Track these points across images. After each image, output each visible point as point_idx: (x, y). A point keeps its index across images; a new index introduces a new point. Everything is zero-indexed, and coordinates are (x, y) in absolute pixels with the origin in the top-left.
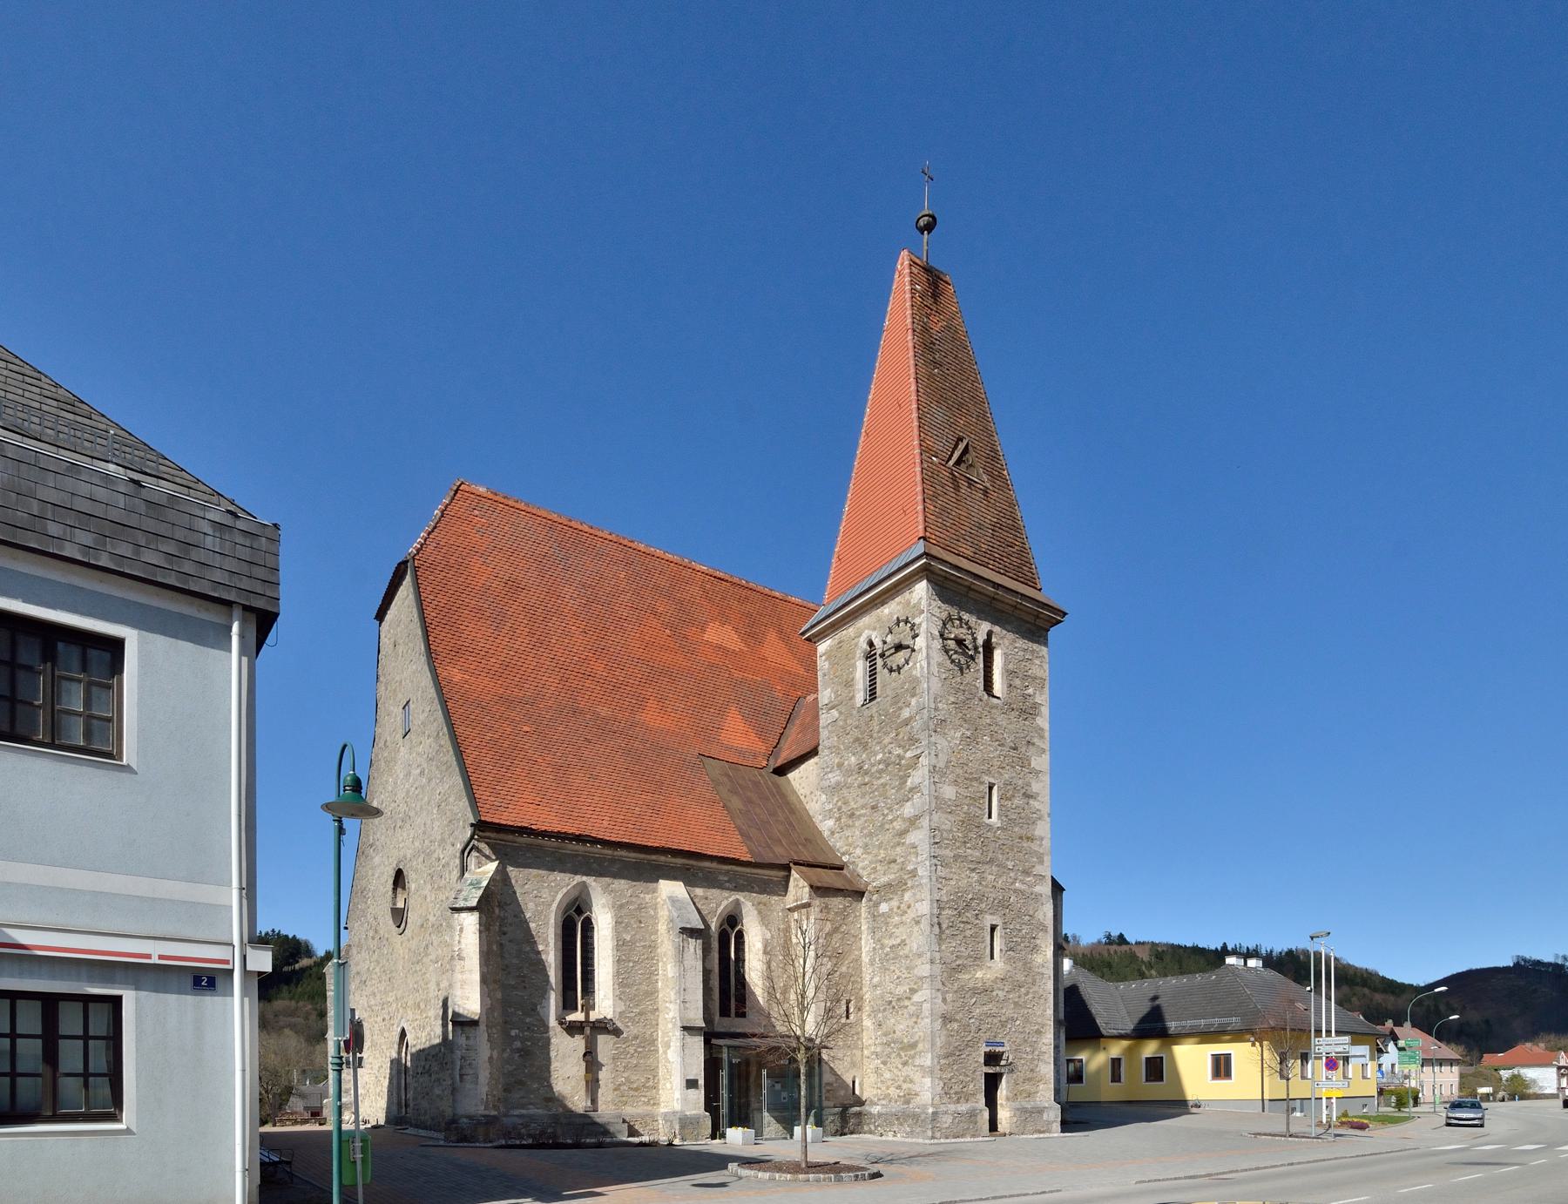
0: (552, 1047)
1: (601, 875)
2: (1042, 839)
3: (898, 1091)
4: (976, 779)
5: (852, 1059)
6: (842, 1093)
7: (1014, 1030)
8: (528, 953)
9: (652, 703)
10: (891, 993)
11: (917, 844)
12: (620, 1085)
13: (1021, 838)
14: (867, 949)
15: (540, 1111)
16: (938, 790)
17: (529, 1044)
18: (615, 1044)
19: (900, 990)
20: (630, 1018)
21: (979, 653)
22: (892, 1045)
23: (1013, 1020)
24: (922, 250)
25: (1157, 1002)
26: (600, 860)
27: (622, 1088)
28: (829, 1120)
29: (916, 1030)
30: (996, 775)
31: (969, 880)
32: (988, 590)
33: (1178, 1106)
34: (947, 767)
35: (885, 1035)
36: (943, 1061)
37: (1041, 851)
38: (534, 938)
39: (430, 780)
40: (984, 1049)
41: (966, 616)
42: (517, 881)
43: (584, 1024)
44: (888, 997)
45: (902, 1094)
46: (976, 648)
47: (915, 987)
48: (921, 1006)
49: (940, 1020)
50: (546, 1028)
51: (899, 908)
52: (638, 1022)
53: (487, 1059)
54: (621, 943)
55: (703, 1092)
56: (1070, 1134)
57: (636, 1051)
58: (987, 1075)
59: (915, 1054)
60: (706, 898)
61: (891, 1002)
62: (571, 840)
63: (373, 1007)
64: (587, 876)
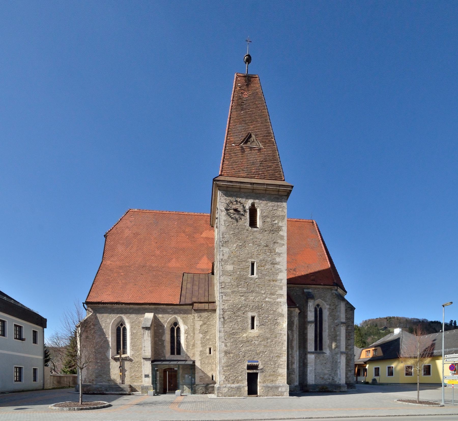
0: (111, 365)
1: (126, 313)
2: (281, 280)
4: (244, 261)
5: (211, 368)
6: (207, 379)
7: (264, 356)
9: (174, 260)
12: (132, 376)
13: (269, 281)
15: (107, 384)
16: (224, 267)
20: (136, 356)
21: (247, 212)
23: (263, 352)
24: (246, 69)
25: (435, 342)
26: (126, 309)
27: (133, 377)
30: (255, 258)
31: (240, 300)
33: (438, 385)
34: (228, 258)
36: (225, 368)
37: (281, 285)
38: (105, 333)
40: (247, 363)
41: (239, 200)
42: (99, 318)
46: (245, 211)
49: (224, 353)
50: (109, 360)
52: (138, 357)
56: (292, 397)
57: (138, 366)
58: (248, 374)
60: (163, 317)
62: (114, 304)
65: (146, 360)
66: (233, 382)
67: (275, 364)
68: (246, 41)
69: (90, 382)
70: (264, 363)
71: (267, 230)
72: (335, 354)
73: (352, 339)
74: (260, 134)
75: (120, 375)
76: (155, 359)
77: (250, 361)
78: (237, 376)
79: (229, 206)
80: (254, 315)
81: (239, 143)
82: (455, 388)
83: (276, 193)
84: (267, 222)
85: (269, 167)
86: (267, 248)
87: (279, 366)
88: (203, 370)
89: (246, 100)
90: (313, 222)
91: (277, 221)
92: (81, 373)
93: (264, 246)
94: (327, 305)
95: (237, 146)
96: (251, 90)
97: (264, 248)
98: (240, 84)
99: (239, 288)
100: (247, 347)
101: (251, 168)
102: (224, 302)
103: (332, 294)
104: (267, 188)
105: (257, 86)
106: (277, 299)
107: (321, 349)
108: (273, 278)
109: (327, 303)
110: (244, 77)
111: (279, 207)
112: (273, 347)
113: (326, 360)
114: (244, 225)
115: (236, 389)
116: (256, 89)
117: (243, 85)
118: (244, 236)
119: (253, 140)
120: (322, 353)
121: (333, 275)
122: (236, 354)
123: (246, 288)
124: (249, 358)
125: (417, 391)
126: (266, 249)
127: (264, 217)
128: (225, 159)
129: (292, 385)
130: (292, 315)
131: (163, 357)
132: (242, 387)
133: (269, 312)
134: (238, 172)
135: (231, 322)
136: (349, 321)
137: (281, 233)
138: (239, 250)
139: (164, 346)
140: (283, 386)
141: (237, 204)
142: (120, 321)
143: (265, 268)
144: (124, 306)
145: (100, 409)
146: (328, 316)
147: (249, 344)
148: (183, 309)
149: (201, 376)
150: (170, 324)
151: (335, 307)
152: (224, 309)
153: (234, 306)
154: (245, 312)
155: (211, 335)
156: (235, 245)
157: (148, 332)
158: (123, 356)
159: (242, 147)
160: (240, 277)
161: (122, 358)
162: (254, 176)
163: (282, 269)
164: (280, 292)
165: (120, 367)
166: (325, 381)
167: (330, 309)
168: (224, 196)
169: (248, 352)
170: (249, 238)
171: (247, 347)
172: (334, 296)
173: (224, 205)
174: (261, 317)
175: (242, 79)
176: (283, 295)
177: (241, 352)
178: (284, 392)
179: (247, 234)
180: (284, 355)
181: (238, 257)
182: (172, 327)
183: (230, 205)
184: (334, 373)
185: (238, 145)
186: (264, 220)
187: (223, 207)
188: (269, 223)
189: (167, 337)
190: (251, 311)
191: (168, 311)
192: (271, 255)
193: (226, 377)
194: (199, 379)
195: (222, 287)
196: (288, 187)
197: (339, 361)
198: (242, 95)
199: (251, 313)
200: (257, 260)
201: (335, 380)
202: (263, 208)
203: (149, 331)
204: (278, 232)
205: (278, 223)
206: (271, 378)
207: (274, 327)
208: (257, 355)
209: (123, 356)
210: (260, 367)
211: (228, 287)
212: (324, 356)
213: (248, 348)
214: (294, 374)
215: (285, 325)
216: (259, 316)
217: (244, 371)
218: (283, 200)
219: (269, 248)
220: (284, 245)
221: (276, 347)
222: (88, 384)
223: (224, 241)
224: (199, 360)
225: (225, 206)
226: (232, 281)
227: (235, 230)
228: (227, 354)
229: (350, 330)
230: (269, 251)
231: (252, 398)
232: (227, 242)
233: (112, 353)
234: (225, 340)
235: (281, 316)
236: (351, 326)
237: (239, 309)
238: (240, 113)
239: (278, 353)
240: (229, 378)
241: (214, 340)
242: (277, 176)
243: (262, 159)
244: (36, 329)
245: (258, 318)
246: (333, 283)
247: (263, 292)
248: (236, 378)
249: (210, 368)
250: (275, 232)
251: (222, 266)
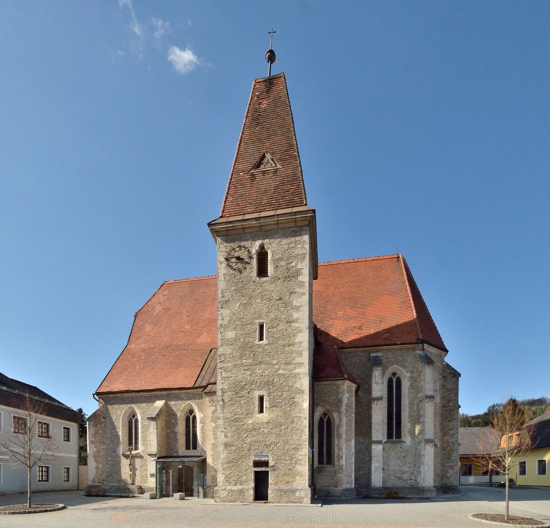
0: (121, 463)
1: (137, 403)
2: (301, 343)
4: (250, 324)
7: (276, 448)
8: (114, 432)
12: (143, 476)
13: (283, 346)
16: (223, 335)
17: (114, 462)
18: (141, 461)
21: (253, 258)
26: (136, 398)
27: (143, 477)
28: (211, 491)
30: (265, 317)
31: (244, 375)
32: (252, 224)
34: (229, 323)
36: (225, 466)
37: (300, 349)
38: (116, 427)
40: (253, 458)
41: (242, 244)
46: (251, 257)
49: (223, 446)
54: (143, 426)
58: (256, 473)
60: (176, 405)
62: (124, 393)
64: (132, 404)
65: (152, 456)
66: (236, 483)
67: (292, 459)
68: (269, 33)
69: (99, 482)
70: (276, 458)
71: (280, 277)
72: (419, 443)
73: (454, 419)
74: (278, 150)
75: (130, 474)
76: (167, 455)
77: (257, 456)
78: (241, 476)
79: (231, 255)
80: (263, 393)
81: (249, 170)
83: (293, 225)
84: (281, 266)
85: (286, 192)
86: (281, 302)
87: (298, 462)
88: (215, 468)
89: (264, 110)
90: (398, 257)
91: (294, 263)
92: (30, 472)
93: (276, 300)
94: (407, 372)
95: (246, 174)
96: (272, 95)
97: (277, 303)
98: (258, 92)
99: (243, 360)
100: (253, 436)
101: (261, 199)
102: (224, 380)
103: (415, 355)
104: (278, 220)
105: (281, 88)
106: (295, 370)
107: (399, 436)
108: (290, 342)
109: (407, 369)
110: (264, 82)
111: (298, 243)
112: (288, 435)
113: (405, 452)
114: (249, 276)
115: (238, 493)
116: (279, 92)
117: (263, 92)
118: (250, 291)
119: (268, 161)
120: (399, 442)
121: (418, 327)
122: (239, 447)
123: (253, 359)
124: (256, 451)
125: (505, 502)
126: (279, 303)
127: (276, 261)
128: (228, 195)
129: (340, 488)
130: (340, 390)
131: (176, 452)
132: (245, 490)
133: (283, 388)
134: (243, 208)
135: (232, 406)
136: (450, 393)
137: (300, 278)
138: (243, 310)
139: (177, 439)
140: (302, 490)
141: (240, 250)
142: (132, 412)
143: (278, 329)
144: (135, 394)
145: (39, 513)
146: (409, 389)
147: (255, 433)
148: (198, 392)
149: (213, 476)
150: (185, 413)
151: (418, 374)
152: (223, 390)
153: (236, 384)
154: (250, 391)
156: (238, 305)
157: (154, 424)
158: (134, 452)
159: (252, 174)
160: (244, 345)
161: (132, 454)
162: (264, 208)
163: (301, 328)
164: (298, 360)
165: (130, 465)
166: (403, 483)
167: (411, 377)
168: (224, 243)
169: (254, 444)
170: (256, 292)
171: (253, 436)
172: (417, 358)
173: (224, 254)
174: (272, 397)
175: (262, 84)
176: (303, 363)
177: (245, 443)
178: (304, 498)
179: (253, 287)
180: (304, 446)
181: (242, 320)
182: (188, 416)
183: (232, 254)
184: (417, 471)
185: (247, 172)
186: (277, 265)
187: (222, 258)
188: (284, 267)
189: (181, 428)
190: (259, 389)
191: (181, 397)
192: (286, 311)
193: (226, 477)
194: (211, 479)
195: (221, 360)
196: (309, 213)
197: (422, 453)
198: (260, 106)
199: (258, 392)
200: (267, 320)
201: (419, 481)
202: (275, 249)
203: (155, 422)
204: (297, 277)
205: (296, 265)
206: (286, 478)
207: (289, 408)
208: (267, 447)
209: (134, 452)
210: (271, 463)
211: (229, 359)
212: (403, 447)
213: (254, 439)
214: (342, 472)
215: (306, 405)
216: (269, 395)
217: (250, 469)
218: (303, 232)
219: (284, 302)
220: (304, 294)
221: (293, 436)
222: (98, 484)
223: (224, 300)
224: (211, 455)
225: (225, 255)
226: (234, 352)
227: (238, 284)
228: (228, 446)
229: (451, 406)
230: (284, 306)
231: (260, 505)
232: (228, 302)
233: (122, 450)
234: (225, 428)
235: (299, 393)
236: (454, 400)
237: (243, 388)
238: (255, 130)
239: (296, 444)
240: (231, 478)
242: (296, 202)
243: (277, 183)
244: (68, 426)
245: (268, 398)
246: (416, 340)
247: (275, 362)
248: (240, 478)
250: (292, 278)
251: (221, 333)
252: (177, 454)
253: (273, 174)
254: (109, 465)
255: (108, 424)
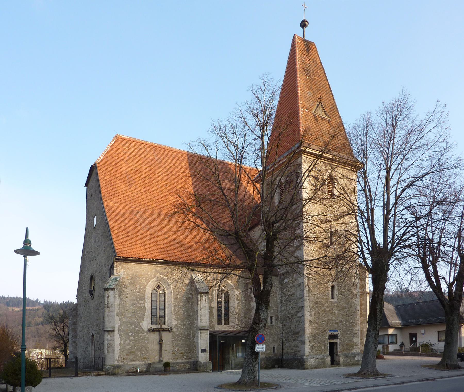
3: (292, 350)
8: (137, 304)
10: (289, 313)
11: (299, 256)
14: (279, 297)
15: (141, 363)
17: (137, 338)
19: (293, 312)
22: (289, 333)
29: (299, 327)
35: (287, 329)
39: (101, 243)
43: (159, 330)
44: (288, 315)
45: (293, 352)
47: (299, 310)
48: (301, 318)
51: (292, 280)
53: (118, 344)
55: (209, 353)
57: (181, 339)
58: (330, 344)
59: (298, 336)
61: (289, 317)
63: (84, 326)
82: (29, 310)
155: (273, 303)
241: (276, 308)
249: (272, 339)
252: (213, 329)
253: (455, 245)
254: (130, 341)
255: (129, 294)
